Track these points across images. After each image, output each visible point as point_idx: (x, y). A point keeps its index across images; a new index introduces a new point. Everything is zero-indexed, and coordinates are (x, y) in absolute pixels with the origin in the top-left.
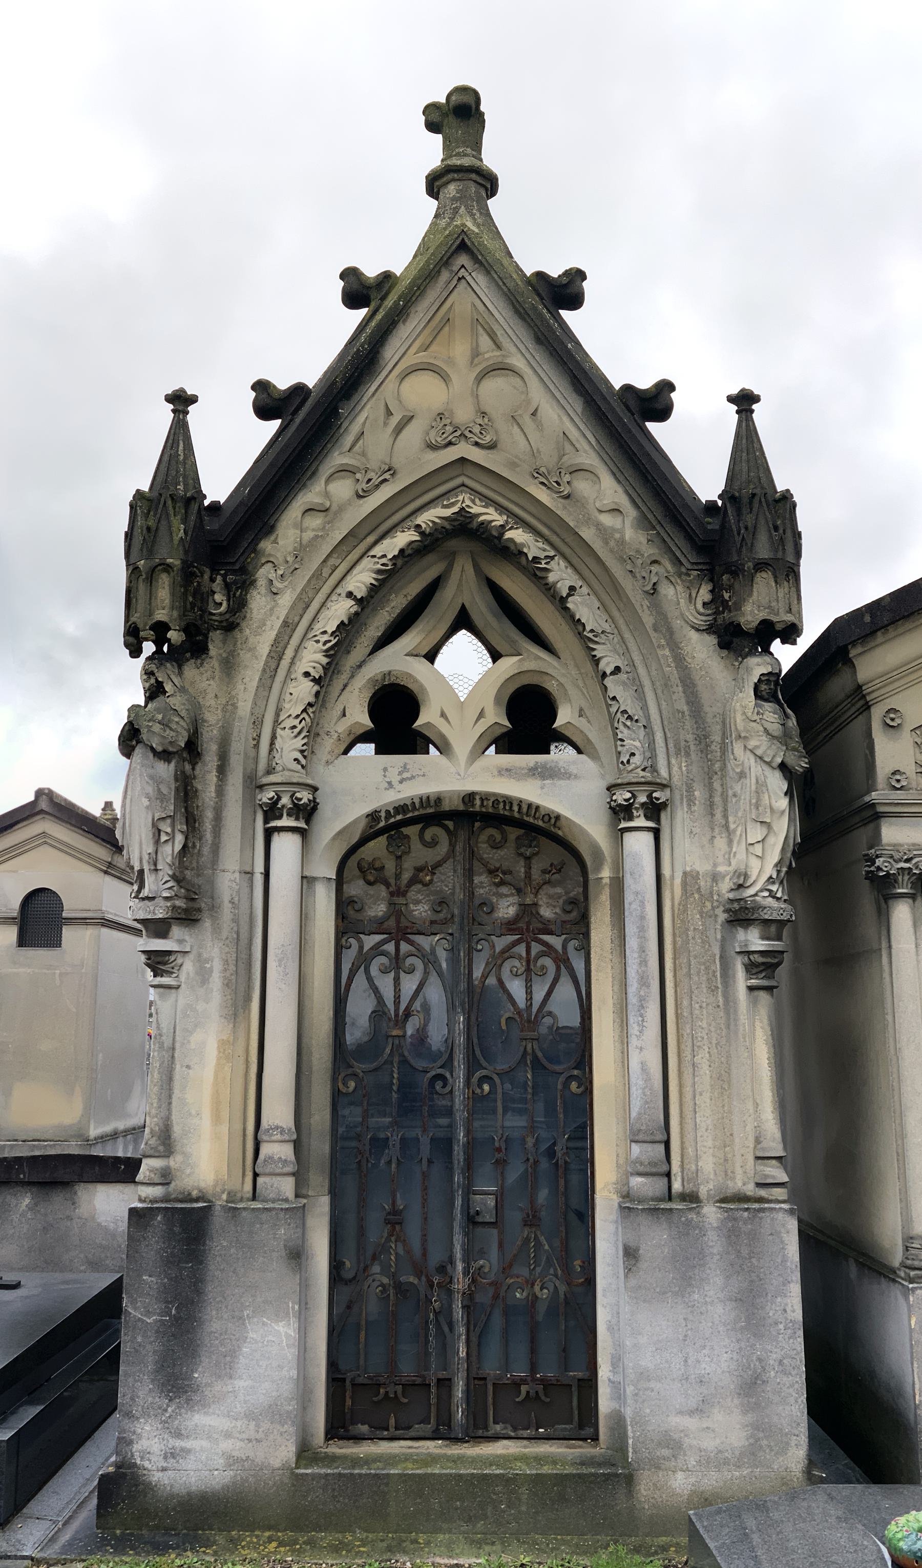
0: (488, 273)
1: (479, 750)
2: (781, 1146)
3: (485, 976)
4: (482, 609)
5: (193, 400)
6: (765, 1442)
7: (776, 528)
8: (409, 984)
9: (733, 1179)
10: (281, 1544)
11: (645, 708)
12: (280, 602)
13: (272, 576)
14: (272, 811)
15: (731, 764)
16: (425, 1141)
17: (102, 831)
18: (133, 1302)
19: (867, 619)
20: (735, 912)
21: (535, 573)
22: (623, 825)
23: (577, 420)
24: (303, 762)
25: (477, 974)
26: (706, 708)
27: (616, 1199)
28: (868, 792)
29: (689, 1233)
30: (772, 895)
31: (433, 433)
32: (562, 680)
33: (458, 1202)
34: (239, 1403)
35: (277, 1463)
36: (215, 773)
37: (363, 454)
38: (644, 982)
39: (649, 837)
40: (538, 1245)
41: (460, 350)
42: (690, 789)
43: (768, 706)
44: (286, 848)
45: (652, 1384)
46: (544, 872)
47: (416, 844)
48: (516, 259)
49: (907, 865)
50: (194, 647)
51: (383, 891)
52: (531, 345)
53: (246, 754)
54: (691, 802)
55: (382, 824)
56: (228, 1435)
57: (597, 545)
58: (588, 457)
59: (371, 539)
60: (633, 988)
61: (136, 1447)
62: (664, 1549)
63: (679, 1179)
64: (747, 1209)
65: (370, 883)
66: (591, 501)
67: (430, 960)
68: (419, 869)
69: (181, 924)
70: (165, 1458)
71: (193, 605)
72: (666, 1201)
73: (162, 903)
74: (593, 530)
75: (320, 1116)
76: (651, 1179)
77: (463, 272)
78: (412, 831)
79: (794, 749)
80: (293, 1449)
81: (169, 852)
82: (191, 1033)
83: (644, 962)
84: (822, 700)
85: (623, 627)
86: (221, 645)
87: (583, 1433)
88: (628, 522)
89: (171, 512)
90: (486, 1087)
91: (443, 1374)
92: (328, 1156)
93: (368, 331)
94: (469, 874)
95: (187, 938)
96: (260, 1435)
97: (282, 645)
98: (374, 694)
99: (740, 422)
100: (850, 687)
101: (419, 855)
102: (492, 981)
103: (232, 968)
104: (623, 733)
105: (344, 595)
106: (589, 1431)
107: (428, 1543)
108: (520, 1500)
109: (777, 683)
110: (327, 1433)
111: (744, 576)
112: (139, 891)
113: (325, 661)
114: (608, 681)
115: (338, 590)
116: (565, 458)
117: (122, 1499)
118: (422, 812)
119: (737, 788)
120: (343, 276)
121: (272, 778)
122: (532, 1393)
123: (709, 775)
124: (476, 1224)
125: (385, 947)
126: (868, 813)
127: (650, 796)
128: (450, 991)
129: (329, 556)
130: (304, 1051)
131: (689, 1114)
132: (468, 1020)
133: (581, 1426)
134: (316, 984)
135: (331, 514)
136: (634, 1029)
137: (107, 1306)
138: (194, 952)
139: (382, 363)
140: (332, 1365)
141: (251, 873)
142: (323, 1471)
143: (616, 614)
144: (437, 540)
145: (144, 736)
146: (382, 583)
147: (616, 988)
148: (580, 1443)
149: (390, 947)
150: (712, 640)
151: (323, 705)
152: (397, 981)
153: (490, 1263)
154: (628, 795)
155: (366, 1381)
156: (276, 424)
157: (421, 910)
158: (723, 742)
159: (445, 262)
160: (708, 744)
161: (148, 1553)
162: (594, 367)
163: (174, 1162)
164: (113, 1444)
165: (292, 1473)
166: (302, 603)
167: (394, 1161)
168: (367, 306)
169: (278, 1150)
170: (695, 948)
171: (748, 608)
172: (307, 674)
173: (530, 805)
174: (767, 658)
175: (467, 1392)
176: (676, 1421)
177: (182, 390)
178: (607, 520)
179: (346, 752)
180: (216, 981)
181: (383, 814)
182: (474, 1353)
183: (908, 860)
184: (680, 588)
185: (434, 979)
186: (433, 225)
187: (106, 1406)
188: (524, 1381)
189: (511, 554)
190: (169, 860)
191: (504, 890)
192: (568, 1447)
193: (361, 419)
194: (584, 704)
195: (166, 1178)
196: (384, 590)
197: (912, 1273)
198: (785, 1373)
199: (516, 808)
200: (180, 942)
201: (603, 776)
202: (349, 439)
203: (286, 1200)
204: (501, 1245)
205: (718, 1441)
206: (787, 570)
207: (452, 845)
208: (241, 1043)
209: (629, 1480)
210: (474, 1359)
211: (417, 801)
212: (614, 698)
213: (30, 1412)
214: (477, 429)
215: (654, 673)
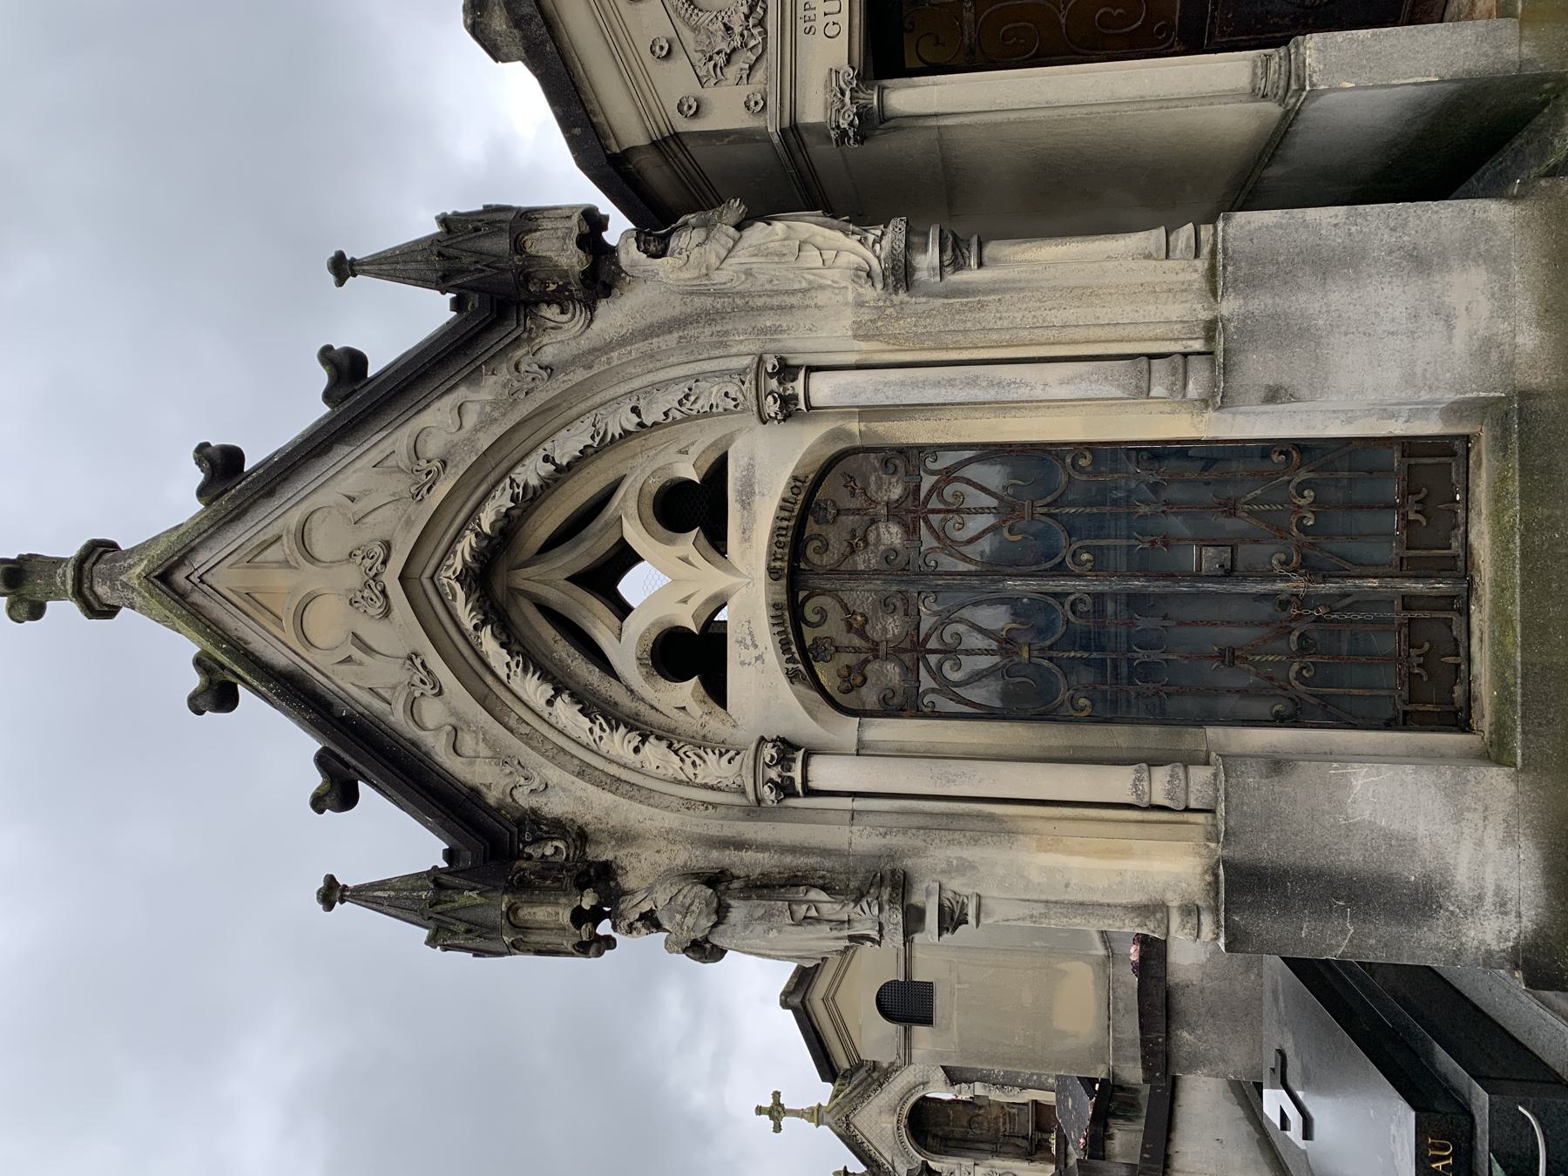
0: (193, 550)
1: (730, 569)
2: (1154, 232)
6: (1482, 247)
9: (1190, 283)
11: (675, 381)
12: (555, 780)
13: (526, 790)
14: (785, 789)
18: (1331, 947)
19: (577, 131)
20: (897, 281)
21: (530, 500)
22: (802, 405)
23: (358, 452)
24: (732, 753)
25: (963, 567)
26: (676, 313)
27: (1210, 414)
29: (1249, 330)
30: (879, 240)
31: (371, 611)
32: (648, 472)
33: (1211, 587)
34: (1421, 819)
35: (1511, 788)
37: (394, 688)
38: (973, 382)
39: (816, 377)
40: (1255, 500)
41: (280, 580)
42: (763, 331)
43: (673, 243)
44: (824, 773)
45: (1419, 370)
46: (853, 494)
49: (848, 94)
50: (602, 877)
53: (724, 818)
54: (777, 330)
55: (801, 667)
56: (1480, 843)
57: (498, 430)
58: (400, 440)
59: (489, 679)
60: (981, 395)
61: (1494, 947)
63: (1190, 343)
64: (1224, 267)
65: (865, 680)
66: (450, 437)
68: (850, 627)
69: (909, 892)
70: (1506, 913)
71: (557, 879)
72: (1215, 356)
73: (885, 915)
74: (481, 435)
75: (1119, 736)
76: (1191, 374)
78: (809, 635)
79: (720, 216)
80: (1494, 770)
81: (830, 907)
83: (951, 382)
84: (661, 184)
85: (590, 403)
86: (602, 847)
87: (1460, 450)
89: (449, 905)
90: (1085, 557)
91: (1398, 604)
92: (1163, 729)
93: (255, 683)
94: (854, 574)
95: (924, 886)
96: (1480, 806)
97: (604, 778)
98: (663, 676)
99: (365, 273)
101: (834, 628)
103: (957, 835)
105: (550, 709)
106: (1458, 446)
108: (1549, 517)
110: (1463, 731)
111: (529, 266)
112: (873, 940)
113: (622, 729)
114: (648, 422)
115: (546, 716)
116: (402, 466)
118: (788, 624)
119: (763, 279)
123: (750, 310)
124: (1233, 569)
126: (792, 140)
127: (771, 375)
129: (505, 726)
130: (1046, 754)
132: (1011, 576)
133: (1454, 454)
135: (459, 724)
136: (1023, 393)
137: (1308, 971)
138: (940, 878)
140: (1388, 725)
141: (853, 811)
142: (1519, 736)
144: (492, 606)
145: (699, 935)
147: (978, 415)
148: (1472, 454)
149: (933, 659)
150: (602, 306)
151: (673, 731)
152: (969, 652)
153: (1271, 554)
154: (770, 398)
155: (1406, 687)
157: (892, 627)
158: (710, 295)
159: (181, 597)
160: (710, 312)
163: (1174, 903)
165: (1522, 770)
166: (558, 755)
167: (1165, 656)
169: (1160, 785)
170: (937, 325)
171: (564, 261)
172: (636, 750)
173: (782, 508)
175: (1417, 578)
176: (1460, 344)
178: (471, 420)
180: (970, 853)
181: (790, 666)
182: (1373, 570)
183: (843, 93)
184: (546, 340)
186: (141, 610)
188: (1404, 516)
189: (509, 527)
190: (837, 907)
191: (872, 537)
192: (1479, 465)
194: (673, 449)
196: (548, 664)
197: (1294, 87)
198: (1404, 226)
199: (785, 523)
200: (928, 894)
202: (377, 705)
203: (1215, 775)
205: (1481, 298)
206: (525, 220)
207: (824, 592)
208: (1039, 825)
209: (1525, 395)
210: (1380, 571)
211: (777, 629)
212: (666, 414)
213: (1444, 1060)
214: (368, 562)
215: (639, 370)
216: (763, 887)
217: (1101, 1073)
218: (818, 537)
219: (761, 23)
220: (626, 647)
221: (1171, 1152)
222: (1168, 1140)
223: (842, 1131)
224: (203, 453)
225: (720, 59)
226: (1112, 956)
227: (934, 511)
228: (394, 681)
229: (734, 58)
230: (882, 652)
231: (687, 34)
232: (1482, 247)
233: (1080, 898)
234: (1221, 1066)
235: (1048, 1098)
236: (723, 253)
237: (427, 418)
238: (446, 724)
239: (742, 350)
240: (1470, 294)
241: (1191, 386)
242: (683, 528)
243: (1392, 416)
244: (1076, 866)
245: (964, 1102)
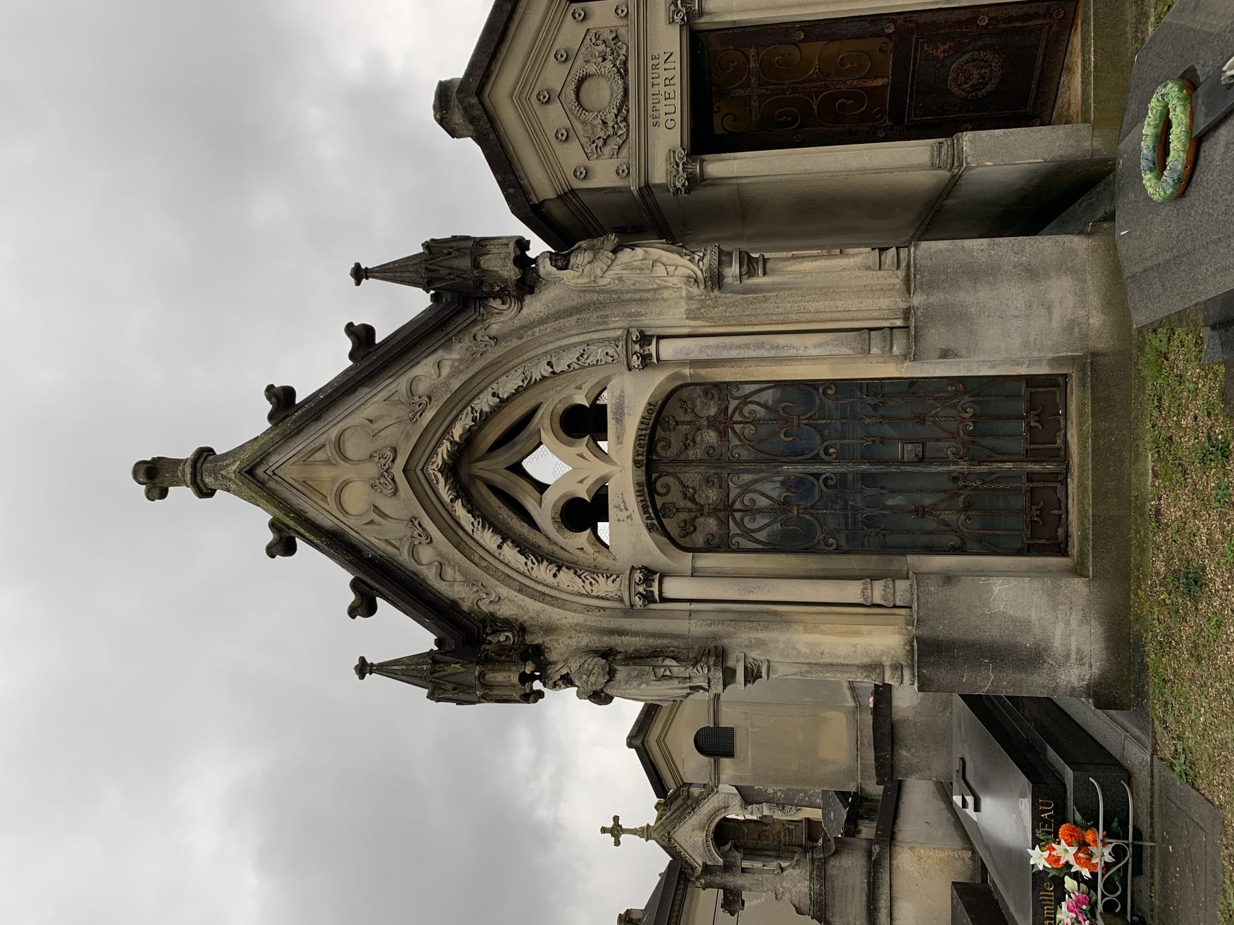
4: (507, 456)
5: (362, 660)
9: (894, 285)
11: (574, 345)
13: (487, 601)
14: (648, 598)
19: (511, 191)
21: (484, 420)
23: (375, 392)
26: (575, 303)
30: (701, 259)
32: (557, 401)
33: (909, 469)
37: (401, 539)
38: (760, 346)
39: (663, 343)
41: (326, 473)
42: (630, 315)
43: (572, 261)
44: (673, 588)
45: (1032, 339)
46: (686, 412)
47: (668, 499)
48: (259, 434)
50: (537, 654)
51: (701, 520)
54: (639, 314)
56: (1068, 623)
57: (464, 378)
58: (402, 384)
59: (461, 533)
61: (1076, 685)
65: (695, 530)
68: (685, 496)
72: (909, 330)
73: (712, 673)
74: (452, 381)
75: (853, 562)
78: (659, 502)
81: (678, 670)
82: (799, 652)
83: (747, 346)
85: (520, 359)
88: (447, 357)
90: (832, 450)
91: (1024, 478)
94: (688, 463)
101: (675, 496)
103: (755, 624)
106: (1060, 380)
107: (1138, 489)
110: (1064, 556)
113: (545, 563)
114: (558, 370)
117: (1104, 695)
121: (626, 598)
123: (621, 302)
124: (923, 458)
125: (738, 431)
126: (645, 193)
127: (635, 342)
132: (787, 463)
133: (1058, 386)
136: (793, 352)
137: (975, 702)
140: (1019, 553)
143: (511, 364)
145: (598, 688)
146: (491, 525)
150: (528, 299)
156: (379, 600)
157: (711, 495)
159: (262, 484)
160: (594, 304)
161: (1147, 676)
163: (887, 662)
166: (506, 579)
169: (878, 592)
171: (505, 274)
172: (555, 576)
173: (642, 423)
174: (540, 261)
175: (1036, 462)
177: (356, 668)
178: (446, 371)
179: (606, 546)
180: (763, 635)
183: (678, 165)
186: (235, 493)
187: (1048, 706)
188: (1028, 424)
191: (698, 439)
193: (376, 541)
194: (573, 386)
196: (495, 522)
198: (1023, 251)
200: (738, 660)
201: (622, 374)
202: (390, 549)
203: (911, 586)
204: (938, 440)
206: (480, 245)
207: (668, 474)
208: (806, 618)
209: (1095, 354)
210: (1014, 458)
213: (1052, 754)
214: (383, 461)
216: (636, 658)
217: (852, 788)
219: (625, 119)
220: (544, 511)
222: (894, 823)
225: (600, 143)
226: (859, 707)
227: (737, 423)
228: (401, 535)
229: (608, 141)
231: (578, 126)
233: (829, 661)
235: (816, 814)
236: (605, 268)
237: (418, 370)
238: (430, 560)
239: (616, 326)
240: (1060, 290)
241: (895, 348)
244: (831, 638)
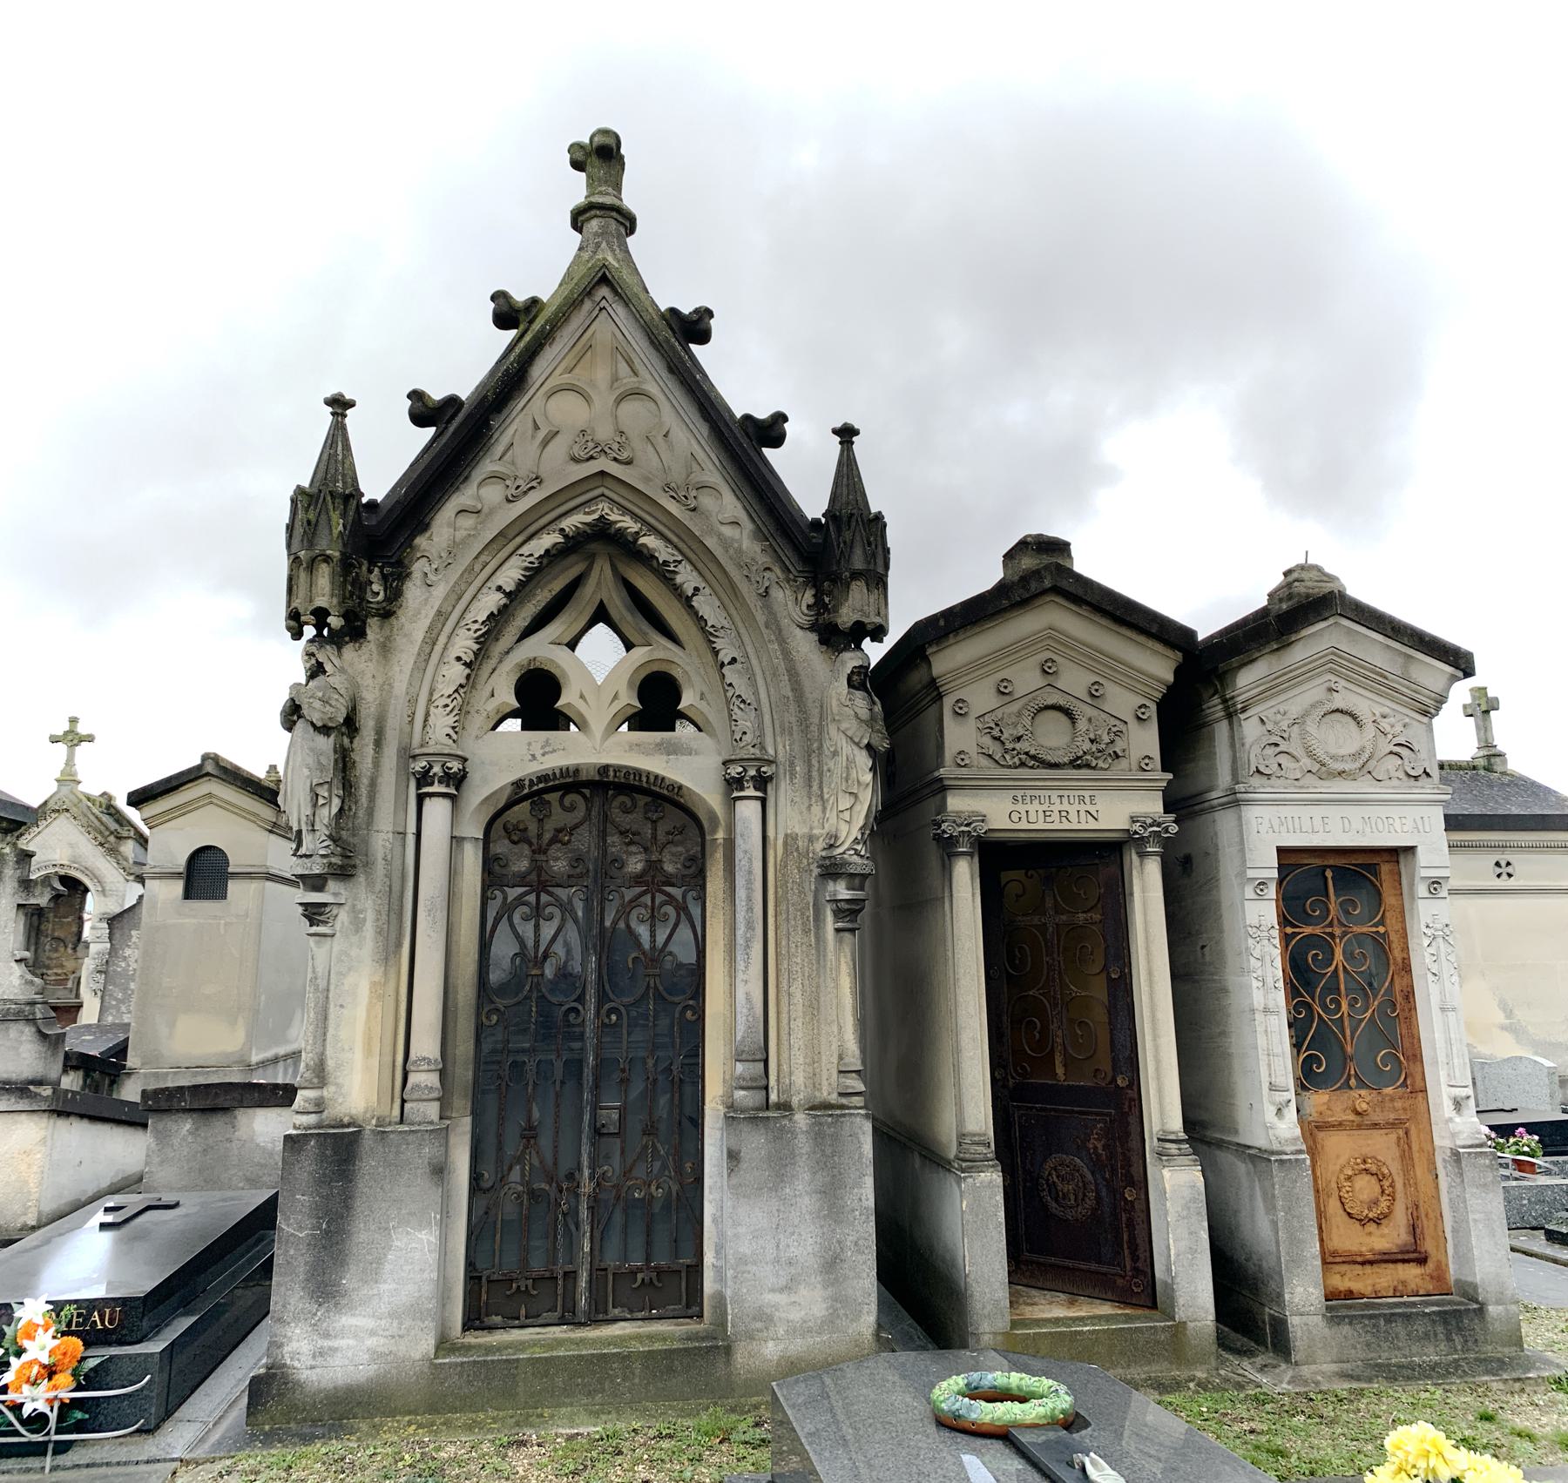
3: (615, 923)
4: (618, 605)
5: (351, 404)
7: (869, 544)
8: (548, 930)
9: (820, 1090)
10: (420, 1426)
11: (756, 693)
14: (424, 778)
15: (827, 744)
16: (559, 1065)
17: (265, 792)
18: (287, 1219)
19: (942, 623)
21: (665, 575)
24: (455, 736)
25: (608, 923)
28: (938, 769)
29: (782, 1136)
30: (857, 853)
32: (687, 668)
33: (587, 1117)
35: (418, 1356)
36: (371, 746)
37: (513, 463)
38: (750, 926)
39: (757, 805)
41: (602, 374)
42: (792, 764)
43: (859, 694)
44: (437, 810)
46: (668, 833)
50: (354, 631)
51: (526, 850)
52: (665, 374)
56: (373, 1333)
57: (718, 552)
59: (519, 540)
60: (740, 932)
61: (286, 1349)
62: (756, 1407)
67: (566, 908)
68: (559, 831)
70: (314, 1357)
71: (352, 594)
72: (763, 1110)
73: (319, 860)
74: (715, 539)
75: (464, 1047)
77: (604, 303)
78: (553, 798)
79: (879, 731)
81: (325, 815)
83: (750, 909)
84: (903, 691)
85: (740, 624)
87: (690, 1312)
89: (331, 507)
90: (614, 1017)
91: (569, 1268)
93: (517, 350)
94: (603, 835)
100: (926, 680)
101: (558, 818)
102: (622, 925)
103: (384, 917)
104: (737, 714)
106: (695, 1309)
107: (552, 1416)
109: (866, 675)
110: (464, 1325)
113: (476, 647)
114: (725, 670)
120: (493, 298)
122: (647, 1280)
123: (809, 754)
125: (642, 899)
126: (936, 786)
127: (758, 771)
128: (584, 935)
131: (784, 1037)
132: (599, 960)
133: (688, 1306)
134: (846, 983)
135: (482, 515)
136: (741, 965)
137: (264, 1219)
139: (530, 381)
140: (470, 1264)
141: (404, 834)
142: (459, 1360)
143: (733, 612)
145: (305, 711)
146: (529, 579)
150: (814, 637)
151: (473, 687)
152: (537, 927)
153: (613, 1168)
157: (559, 865)
159: (588, 292)
160: (808, 726)
161: (295, 1445)
162: (718, 396)
163: (326, 1093)
164: (265, 1346)
168: (516, 327)
169: (423, 1079)
170: (793, 898)
172: (459, 659)
173: (656, 777)
174: (859, 654)
175: (590, 1282)
178: (728, 531)
179: (494, 728)
180: (369, 929)
182: (597, 1247)
185: (570, 925)
186: (577, 257)
187: (261, 1311)
188: (640, 1270)
189: (644, 558)
190: (326, 821)
191: (633, 848)
194: (705, 689)
195: (319, 1106)
196: (531, 586)
198: (860, 1252)
200: (336, 894)
202: (499, 449)
203: (431, 1123)
204: (623, 1152)
206: (878, 581)
207: (589, 810)
208: (392, 984)
209: (728, 1351)
210: (596, 1253)
213: (184, 1323)
214: (615, 447)
217: (132, 1061)
218: (635, 806)
219: (1023, 764)
220: (542, 648)
221: (72, 1119)
222: (82, 1116)
223: (51, 805)
224: (705, 314)
225: (996, 733)
230: (537, 856)
231: (1015, 707)
232: (842, 1312)
233: (332, 1017)
234: (156, 1160)
236: (850, 733)
238: (482, 501)
239: (779, 747)
241: (742, 1093)
242: (641, 698)
243: (718, 1252)
245: (80, 933)
